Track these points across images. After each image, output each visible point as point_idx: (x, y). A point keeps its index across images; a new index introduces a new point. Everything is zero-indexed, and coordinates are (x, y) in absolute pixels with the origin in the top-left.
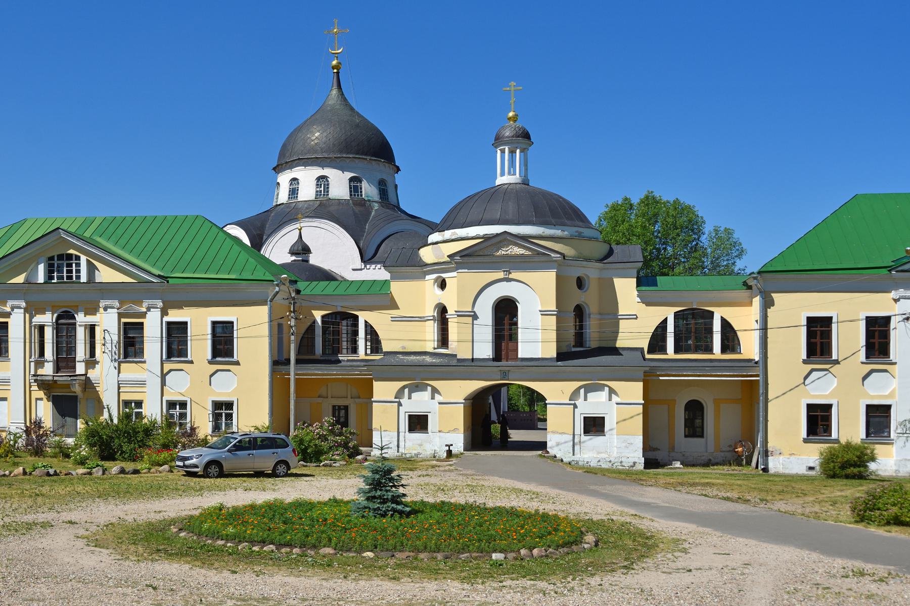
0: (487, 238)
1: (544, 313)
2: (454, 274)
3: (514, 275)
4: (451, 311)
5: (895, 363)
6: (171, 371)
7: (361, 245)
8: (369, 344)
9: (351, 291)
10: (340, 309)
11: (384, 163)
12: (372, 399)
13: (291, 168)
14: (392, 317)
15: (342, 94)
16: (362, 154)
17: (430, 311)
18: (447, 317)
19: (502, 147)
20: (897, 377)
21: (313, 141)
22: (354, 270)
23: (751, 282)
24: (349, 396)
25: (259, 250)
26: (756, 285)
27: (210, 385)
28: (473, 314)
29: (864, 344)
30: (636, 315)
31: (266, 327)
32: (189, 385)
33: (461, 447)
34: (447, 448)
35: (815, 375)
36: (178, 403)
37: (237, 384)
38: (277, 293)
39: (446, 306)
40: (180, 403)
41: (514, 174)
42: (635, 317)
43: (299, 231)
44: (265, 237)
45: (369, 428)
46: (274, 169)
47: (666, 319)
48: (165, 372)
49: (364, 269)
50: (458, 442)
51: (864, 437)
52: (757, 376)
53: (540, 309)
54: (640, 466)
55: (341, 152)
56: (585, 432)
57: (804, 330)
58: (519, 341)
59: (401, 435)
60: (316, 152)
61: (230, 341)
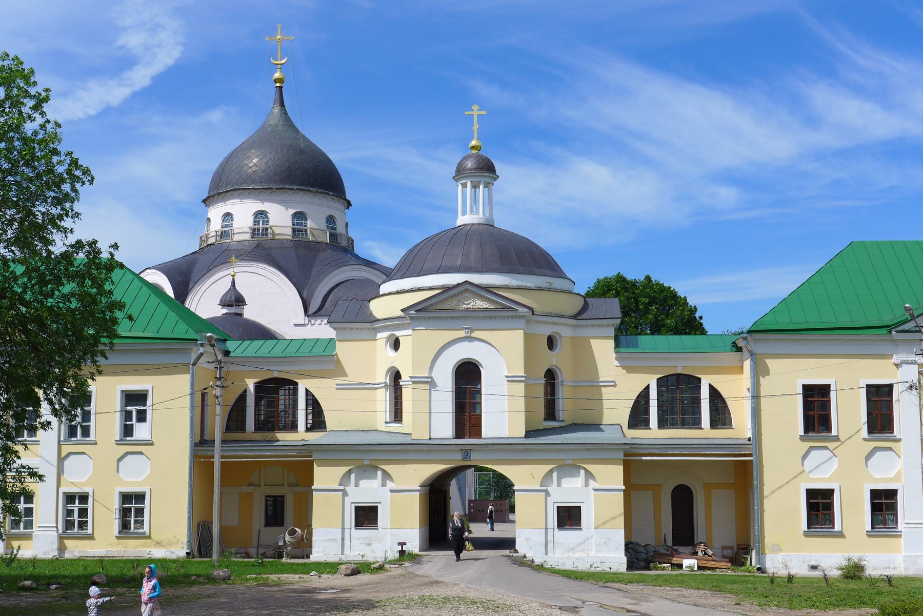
0: (446, 289)
1: (511, 379)
2: (409, 332)
3: (476, 334)
4: (405, 377)
5: (900, 440)
6: (70, 454)
7: (305, 295)
8: (310, 417)
9: (291, 351)
10: (276, 375)
11: (333, 197)
12: (313, 487)
13: (224, 200)
14: (337, 385)
15: (286, 113)
17: (382, 377)
18: (401, 384)
19: (463, 182)
20: (902, 457)
21: (250, 168)
22: (296, 325)
23: (741, 344)
24: (286, 484)
25: (183, 302)
26: (745, 346)
27: (118, 471)
28: (430, 380)
29: (866, 420)
30: (614, 382)
31: (187, 401)
33: (416, 546)
34: (400, 548)
36: (77, 497)
37: (93, 471)
38: (202, 354)
39: (400, 371)
40: (80, 496)
41: (477, 213)
42: (613, 384)
43: (231, 278)
44: (191, 285)
45: (309, 524)
46: (204, 201)
47: (648, 387)
48: (63, 455)
49: (308, 324)
50: (414, 541)
51: (870, 528)
52: (750, 455)
53: (506, 374)
54: (623, 568)
55: (283, 181)
56: (559, 526)
57: (800, 399)
59: (347, 531)
60: (254, 182)
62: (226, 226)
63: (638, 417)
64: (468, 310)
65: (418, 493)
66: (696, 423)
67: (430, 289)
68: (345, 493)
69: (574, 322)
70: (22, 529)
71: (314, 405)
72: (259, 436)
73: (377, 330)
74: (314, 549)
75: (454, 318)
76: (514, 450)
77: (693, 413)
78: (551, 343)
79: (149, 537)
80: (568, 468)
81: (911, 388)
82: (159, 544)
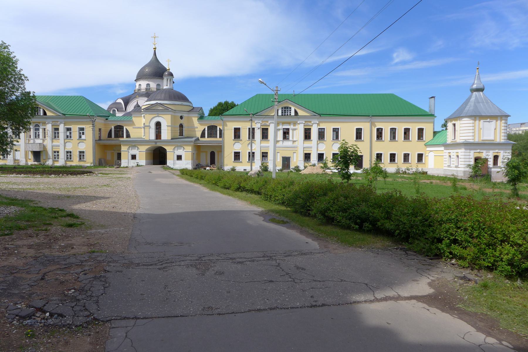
0: (152, 105)
1: (168, 126)
6: (67, 142)
10: (119, 124)
16: (160, 77)
24: (116, 150)
32: (72, 147)
35: (236, 144)
46: (135, 81)
48: (65, 142)
51: (248, 161)
55: (154, 76)
57: (233, 130)
58: (179, 129)
59: (129, 160)
61: (361, 133)
62: (140, 88)
63: (203, 135)
64: (158, 109)
65: (492, 138)
66: (216, 137)
67: (149, 104)
68: (174, 152)
69: (188, 113)
70: (57, 159)
71: (127, 132)
72: (115, 139)
73: (142, 114)
74: (122, 164)
75: (155, 111)
76: (166, 142)
77: (360, 134)
78: (181, 118)
79: (86, 161)
80: (179, 147)
81: (259, 129)
82: (88, 163)
